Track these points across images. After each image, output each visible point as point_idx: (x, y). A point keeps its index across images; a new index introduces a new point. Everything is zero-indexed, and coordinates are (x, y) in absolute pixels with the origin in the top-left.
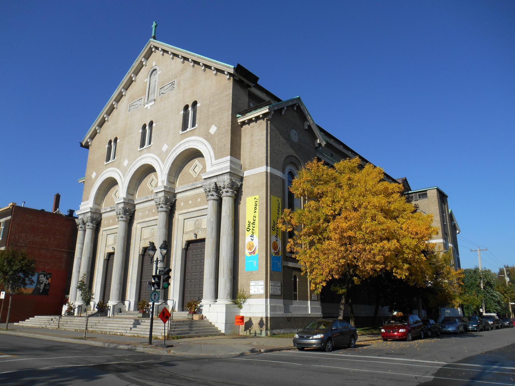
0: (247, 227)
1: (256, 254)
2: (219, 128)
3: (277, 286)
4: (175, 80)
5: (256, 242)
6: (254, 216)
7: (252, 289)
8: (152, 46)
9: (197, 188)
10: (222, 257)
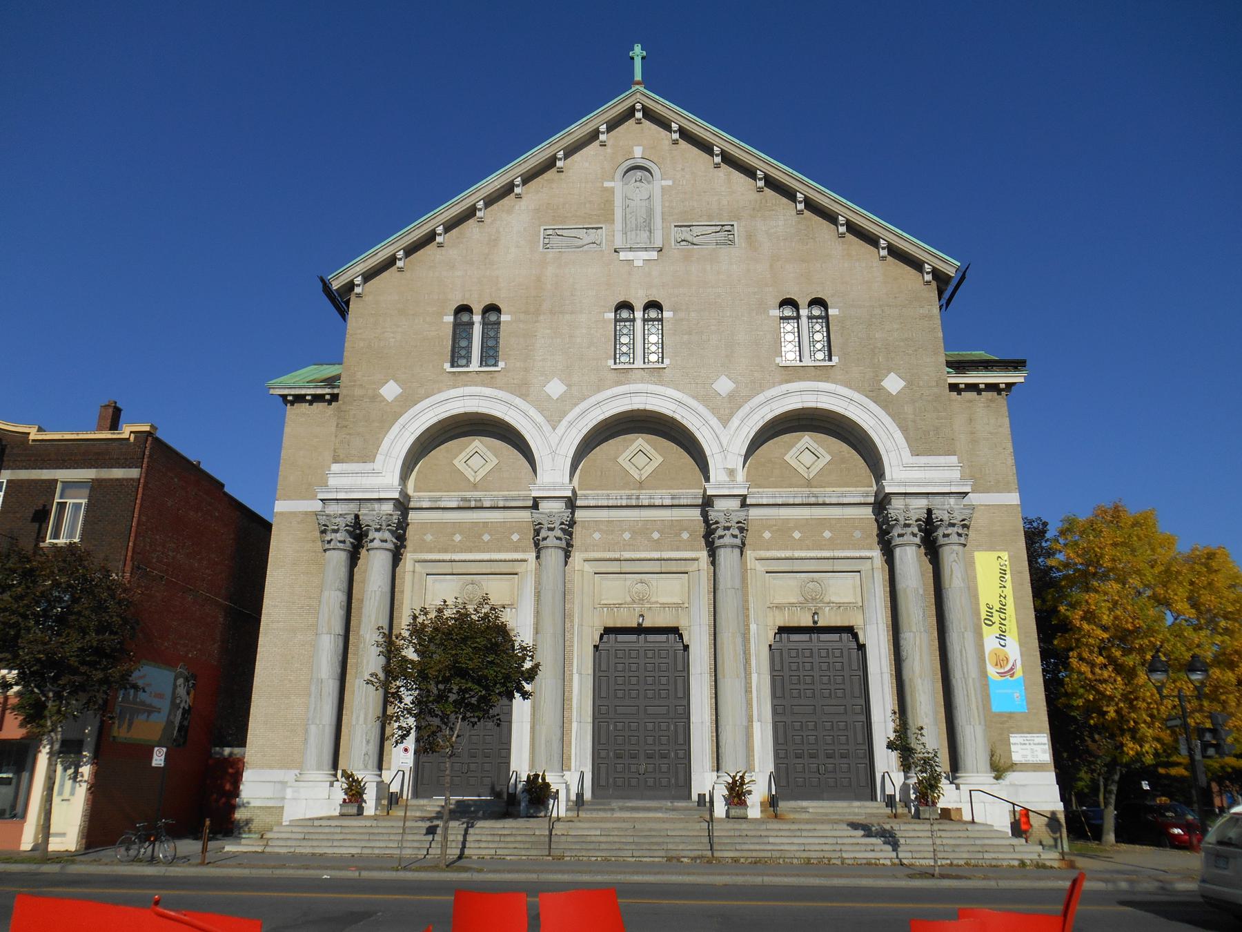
0: (983, 616)
1: (1016, 676)
3: (1035, 744)
4: (735, 224)
5: (1013, 650)
6: (1001, 596)
7: (1017, 752)
8: (638, 106)
9: (824, 504)
10: (971, 681)
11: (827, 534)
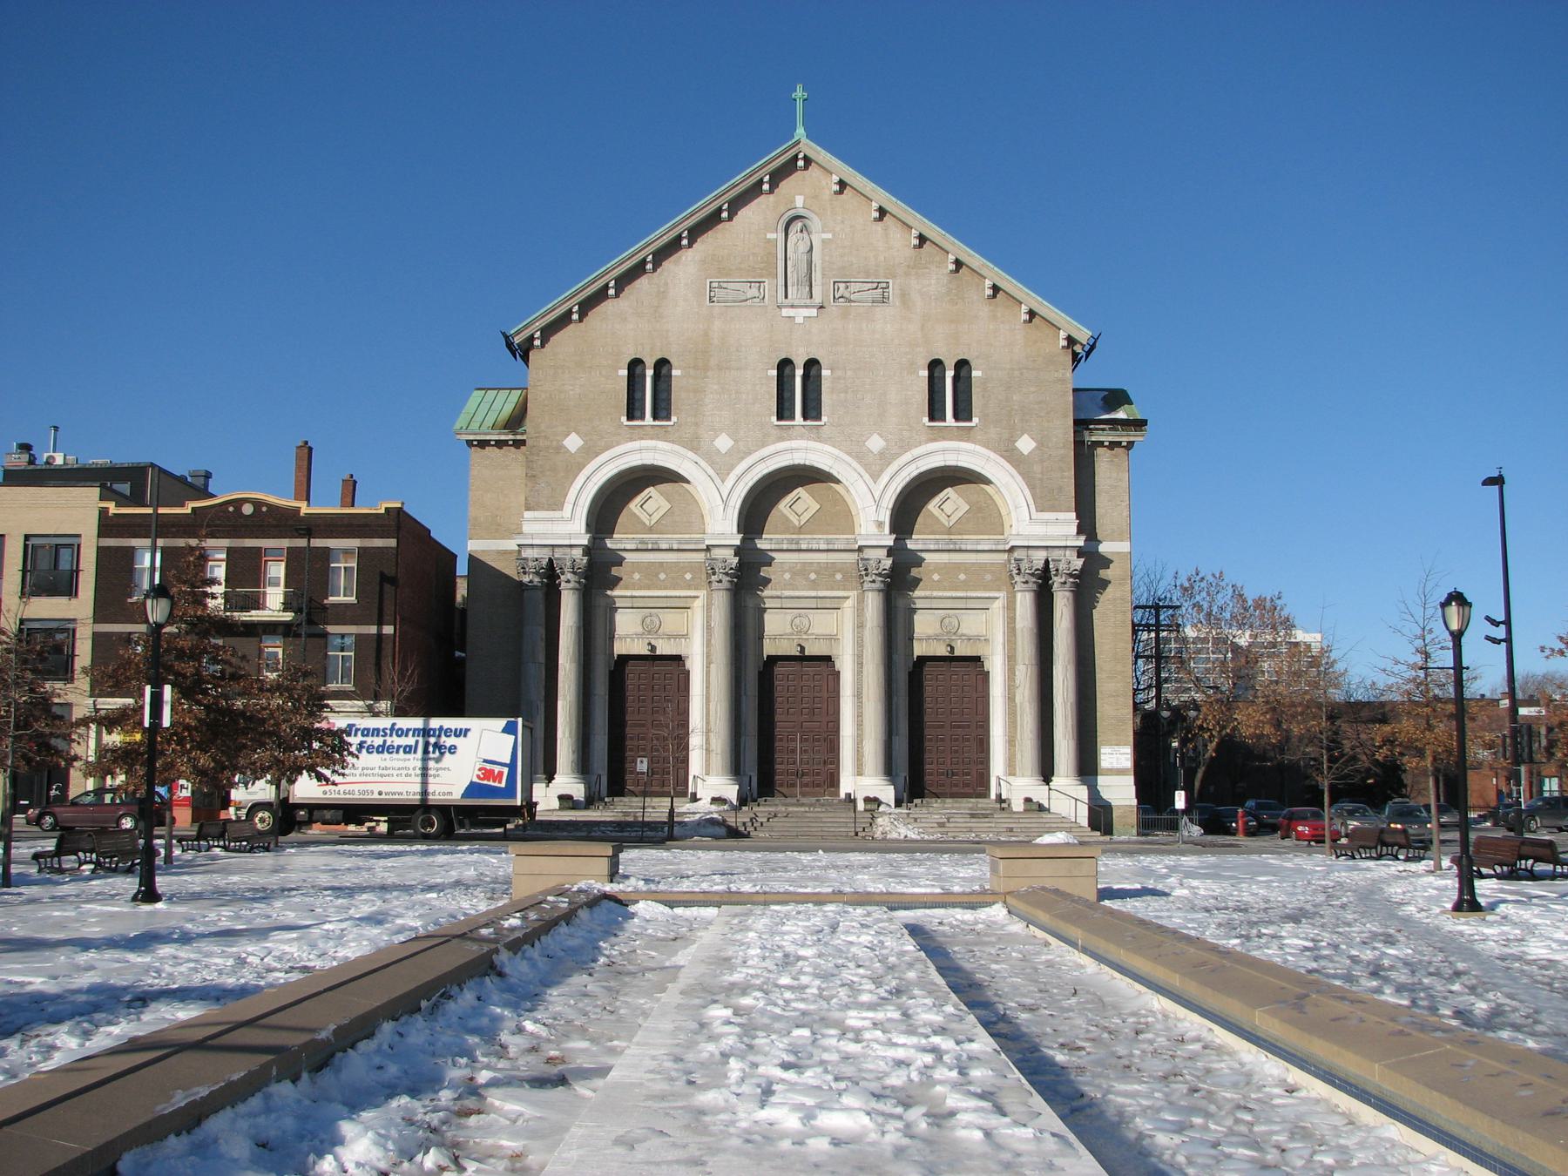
2: (1041, 444)
11: (962, 577)
